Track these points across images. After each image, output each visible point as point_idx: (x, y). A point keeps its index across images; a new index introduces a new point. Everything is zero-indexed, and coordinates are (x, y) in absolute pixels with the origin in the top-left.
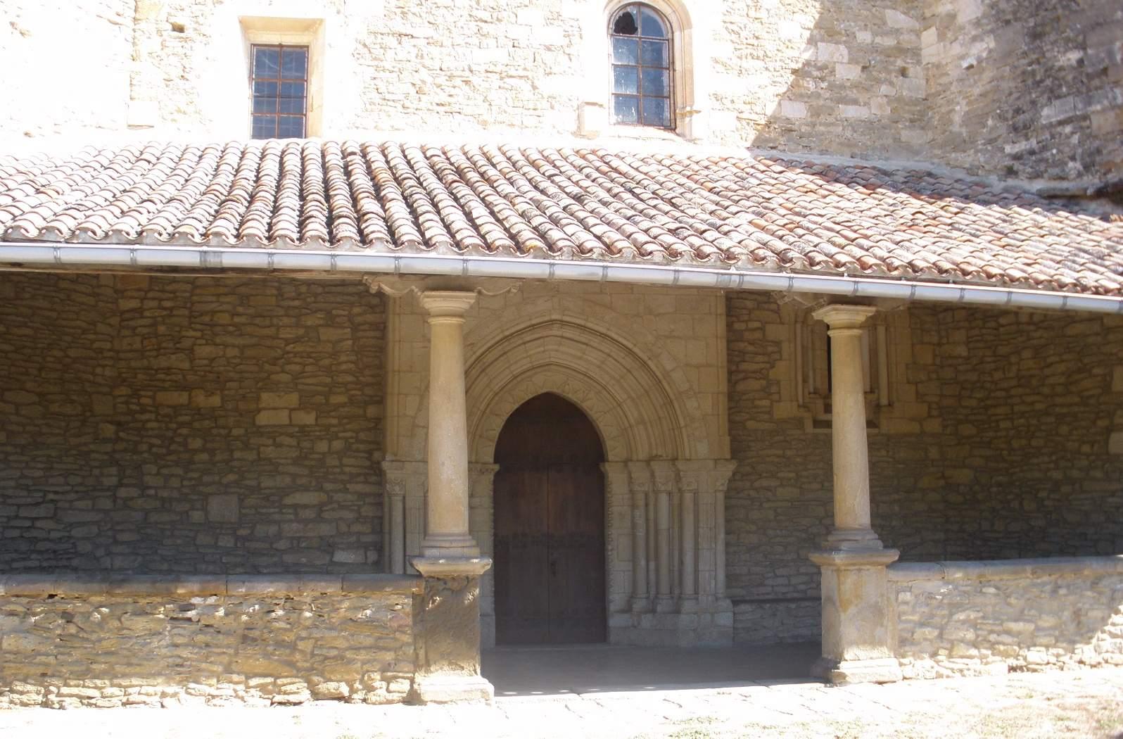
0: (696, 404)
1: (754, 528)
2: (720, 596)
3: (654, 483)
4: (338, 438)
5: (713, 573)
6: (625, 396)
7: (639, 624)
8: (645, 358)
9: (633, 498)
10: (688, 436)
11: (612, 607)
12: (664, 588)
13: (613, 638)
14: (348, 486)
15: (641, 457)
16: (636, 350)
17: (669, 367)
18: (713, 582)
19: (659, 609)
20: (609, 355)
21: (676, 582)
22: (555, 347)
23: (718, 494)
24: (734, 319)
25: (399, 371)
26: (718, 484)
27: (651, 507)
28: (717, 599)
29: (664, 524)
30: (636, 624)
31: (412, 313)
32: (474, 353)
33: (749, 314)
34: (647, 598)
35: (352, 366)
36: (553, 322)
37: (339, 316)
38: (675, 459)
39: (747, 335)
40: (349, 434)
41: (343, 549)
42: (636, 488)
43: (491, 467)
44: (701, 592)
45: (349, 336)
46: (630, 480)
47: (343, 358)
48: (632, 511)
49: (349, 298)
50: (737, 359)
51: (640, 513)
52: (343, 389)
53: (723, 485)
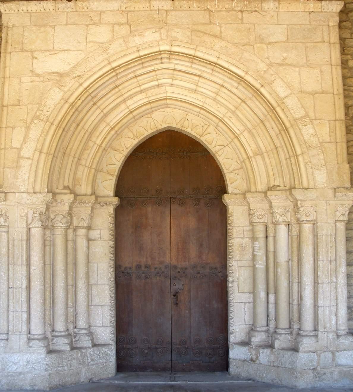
0: (312, 131)
2: (341, 332)
3: (272, 213)
5: (334, 309)
6: (242, 128)
7: (257, 358)
8: (258, 86)
9: (253, 231)
10: (306, 164)
11: (232, 339)
13: (232, 369)
15: (259, 188)
17: (282, 94)
18: (334, 318)
19: (277, 344)
20: (222, 86)
21: (295, 318)
22: (169, 81)
25: (7, 106)
26: (338, 214)
27: (271, 239)
28: (338, 336)
29: (283, 256)
30: (254, 357)
31: (22, 50)
32: (81, 85)
34: (267, 331)
38: (291, 189)
42: (256, 220)
43: (110, 200)
44: (321, 329)
51: (260, 244)
53: (343, 215)
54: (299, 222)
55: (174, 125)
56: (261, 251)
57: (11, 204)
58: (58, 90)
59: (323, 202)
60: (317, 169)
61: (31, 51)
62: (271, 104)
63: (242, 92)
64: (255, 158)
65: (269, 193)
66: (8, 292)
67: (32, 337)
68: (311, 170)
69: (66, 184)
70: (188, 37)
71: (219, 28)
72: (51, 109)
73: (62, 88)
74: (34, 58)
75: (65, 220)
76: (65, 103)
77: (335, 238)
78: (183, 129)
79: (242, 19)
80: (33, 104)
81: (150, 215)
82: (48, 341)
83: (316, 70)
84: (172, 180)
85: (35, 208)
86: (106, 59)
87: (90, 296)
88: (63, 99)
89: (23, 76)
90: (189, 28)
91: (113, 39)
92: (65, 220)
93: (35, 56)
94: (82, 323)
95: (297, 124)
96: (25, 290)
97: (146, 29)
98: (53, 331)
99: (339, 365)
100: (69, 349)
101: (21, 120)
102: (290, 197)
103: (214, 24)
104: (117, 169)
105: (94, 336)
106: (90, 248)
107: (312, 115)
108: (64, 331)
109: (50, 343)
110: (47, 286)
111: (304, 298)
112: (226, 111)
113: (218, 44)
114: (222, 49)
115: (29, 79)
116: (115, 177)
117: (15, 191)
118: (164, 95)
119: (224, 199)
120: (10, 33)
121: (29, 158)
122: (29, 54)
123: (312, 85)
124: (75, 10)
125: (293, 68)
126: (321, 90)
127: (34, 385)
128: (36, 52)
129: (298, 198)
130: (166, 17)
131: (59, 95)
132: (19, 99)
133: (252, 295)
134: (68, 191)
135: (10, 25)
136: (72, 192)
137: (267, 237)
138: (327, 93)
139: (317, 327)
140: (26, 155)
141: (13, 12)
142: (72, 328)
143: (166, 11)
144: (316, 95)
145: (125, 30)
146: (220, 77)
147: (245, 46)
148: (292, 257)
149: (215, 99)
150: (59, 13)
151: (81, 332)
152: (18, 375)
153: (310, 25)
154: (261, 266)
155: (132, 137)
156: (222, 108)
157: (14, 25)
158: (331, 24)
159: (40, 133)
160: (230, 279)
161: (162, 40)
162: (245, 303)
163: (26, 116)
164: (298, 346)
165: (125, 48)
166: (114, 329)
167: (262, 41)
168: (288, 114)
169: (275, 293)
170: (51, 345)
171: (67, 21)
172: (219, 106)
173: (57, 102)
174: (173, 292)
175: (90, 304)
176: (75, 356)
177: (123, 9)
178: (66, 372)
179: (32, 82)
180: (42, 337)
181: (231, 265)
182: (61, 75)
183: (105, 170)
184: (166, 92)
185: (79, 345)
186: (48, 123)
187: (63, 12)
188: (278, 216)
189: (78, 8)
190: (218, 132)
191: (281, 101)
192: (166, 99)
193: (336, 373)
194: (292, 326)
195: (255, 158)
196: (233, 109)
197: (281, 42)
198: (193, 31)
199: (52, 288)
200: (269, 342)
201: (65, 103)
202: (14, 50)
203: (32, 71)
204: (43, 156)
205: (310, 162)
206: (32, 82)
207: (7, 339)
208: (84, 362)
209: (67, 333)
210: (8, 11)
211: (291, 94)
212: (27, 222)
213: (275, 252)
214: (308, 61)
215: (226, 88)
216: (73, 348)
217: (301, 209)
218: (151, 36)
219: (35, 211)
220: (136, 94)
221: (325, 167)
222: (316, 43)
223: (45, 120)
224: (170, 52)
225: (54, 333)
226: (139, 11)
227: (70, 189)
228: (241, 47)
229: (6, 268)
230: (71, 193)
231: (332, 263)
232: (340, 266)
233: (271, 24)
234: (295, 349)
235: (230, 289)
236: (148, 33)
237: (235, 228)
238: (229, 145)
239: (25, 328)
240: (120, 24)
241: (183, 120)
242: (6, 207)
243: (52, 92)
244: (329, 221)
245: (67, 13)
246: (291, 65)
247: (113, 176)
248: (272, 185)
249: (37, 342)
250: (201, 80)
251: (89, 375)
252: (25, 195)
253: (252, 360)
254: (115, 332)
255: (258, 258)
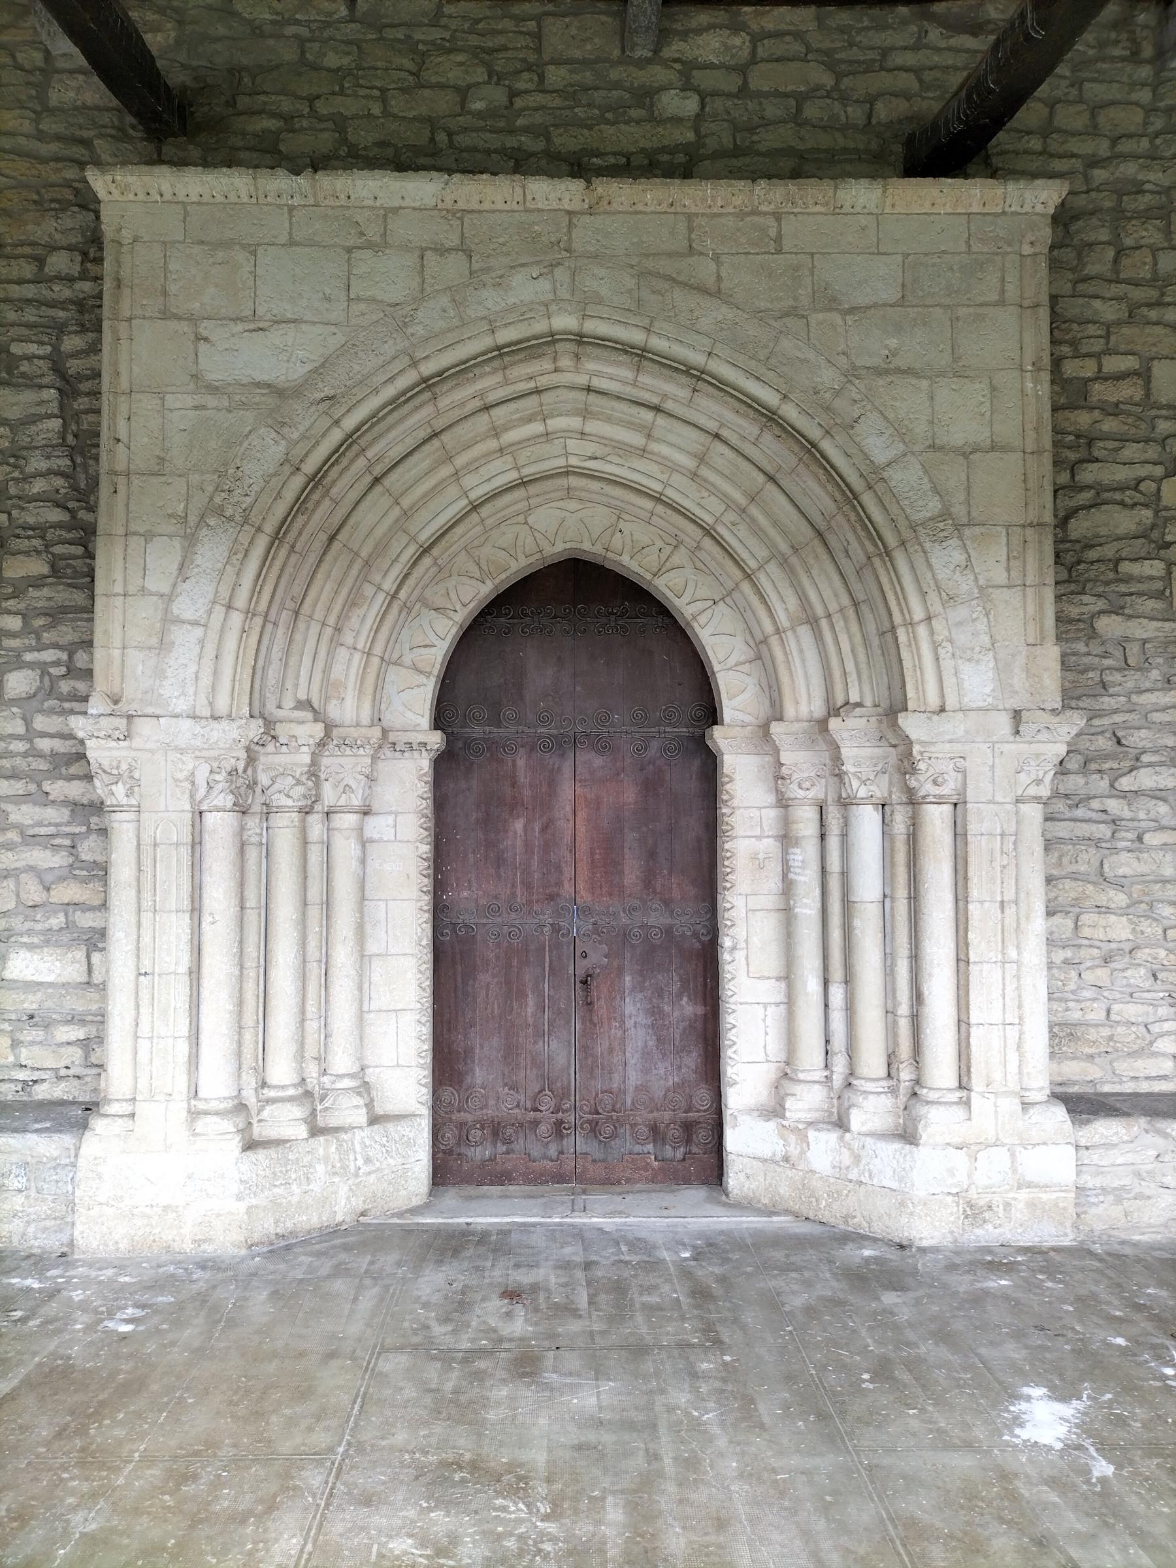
1: (1120, 899)
3: (840, 776)
4: (21, 665)
8: (814, 433)
12: (872, 1061)
13: (734, 1180)
14: (47, 786)
16: (790, 412)
18: (1013, 1057)
19: (857, 1120)
23: (1024, 808)
24: (1066, 349)
31: (166, 315)
33: (1107, 337)
35: (59, 482)
36: (553, 338)
37: (29, 358)
39: (1099, 391)
40: (49, 655)
41: (31, 947)
43: (421, 738)
44: (977, 1084)
45: (54, 408)
46: (778, 776)
47: (37, 463)
48: (785, 852)
49: (51, 312)
50: (1072, 456)
52: (36, 542)
53: (1038, 782)
54: (913, 801)
55: (586, 546)
56: (808, 872)
57: (148, 746)
58: (274, 435)
59: (985, 746)
60: (969, 660)
61: (193, 319)
62: (847, 485)
63: (772, 450)
64: (795, 632)
65: (834, 723)
66: (137, 985)
67: (201, 1106)
68: (952, 662)
69: (302, 696)
70: (630, 291)
71: (713, 266)
72: (255, 488)
73: (286, 430)
74: (199, 338)
75: (300, 790)
76: (292, 473)
77: (1015, 843)
78: (610, 555)
79: (778, 239)
80: (203, 473)
81: (523, 778)
82: (249, 1115)
83: (977, 386)
84: (578, 688)
85: (215, 759)
86: (404, 352)
87: (366, 986)
88: (287, 460)
89: (169, 389)
90: (632, 267)
91: (421, 296)
92: (300, 790)
93: (205, 333)
94: (342, 1061)
95: (917, 538)
96: (187, 978)
97: (512, 267)
98: (264, 1084)
99: (1029, 1185)
100: (305, 1135)
101: (170, 516)
102: (889, 735)
103: (701, 254)
104: (440, 659)
105: (374, 1093)
106: (369, 861)
107: (959, 510)
108: (294, 1086)
109: (254, 1121)
110: (248, 964)
111: (927, 1001)
112: (723, 507)
113: (712, 314)
114: (722, 329)
115: (190, 401)
116: (433, 680)
117: (158, 712)
118: (561, 462)
119: (711, 737)
120: (126, 259)
121: (196, 623)
122: (184, 327)
123: (964, 428)
124: (312, 202)
125: (914, 381)
126: (988, 442)
127: (205, 1241)
128: (206, 323)
129: (913, 737)
130: (569, 232)
131: (277, 451)
132: (162, 455)
133: (783, 985)
134: (309, 715)
135: (126, 235)
136: (318, 716)
137: (823, 837)
138: (1005, 449)
139: (965, 1079)
140: (188, 615)
141: (131, 197)
142: (315, 1075)
143: (569, 213)
144: (975, 457)
145: (453, 268)
146: (711, 410)
147: (787, 320)
148: (893, 889)
149: (694, 476)
150: (266, 208)
151: (339, 1085)
152: (159, 1211)
153: (969, 252)
154: (808, 912)
155: (478, 575)
156: (713, 498)
157: (136, 239)
158: (1027, 250)
159: (226, 554)
160: (726, 942)
161: (557, 300)
162: (765, 1005)
163: (182, 506)
164: (916, 1128)
165: (456, 322)
166: (427, 1072)
167: (831, 303)
168: (894, 509)
169: (846, 982)
170: (255, 1125)
171: (290, 234)
172: (706, 494)
173: (271, 471)
174: (581, 973)
175: (365, 1008)
176: (321, 1151)
177: (449, 204)
178: (295, 1200)
179: (196, 408)
180: (230, 1104)
181: (728, 905)
182: (278, 392)
183: (407, 660)
184: (567, 455)
185: (333, 1121)
186: (246, 527)
187: (279, 206)
188: (855, 784)
189: (321, 196)
190: (699, 564)
191: (875, 476)
192: (567, 473)
193: (1021, 1206)
194: (894, 1072)
195: (795, 632)
196: (742, 501)
197: (885, 305)
198: (643, 274)
199: (262, 971)
200: (831, 1113)
201: (292, 473)
202: (139, 312)
203: (195, 377)
204: (236, 619)
205: (951, 641)
206: (196, 408)
207: (133, 1115)
208: (345, 1168)
209: (300, 1091)
210: (116, 194)
211: (905, 455)
212: (192, 796)
213: (845, 875)
214: (956, 360)
215: (725, 442)
216: (316, 1131)
217: (922, 766)
218: (526, 288)
219: (215, 765)
220: (487, 457)
221: (991, 654)
222: (981, 305)
223: (238, 518)
224: (580, 339)
225: (266, 1091)
226: (494, 212)
227: (314, 710)
228: (772, 322)
229: (133, 920)
230: (316, 720)
231: (1007, 911)
232: (1028, 918)
233: (859, 254)
234: (907, 1135)
235: (728, 967)
236: (517, 279)
237: (738, 812)
238: (728, 600)
239: (181, 1084)
240: (442, 251)
241: (609, 531)
242: (133, 754)
243: (254, 440)
244: (999, 798)
245: (291, 209)
246: (908, 372)
247: (428, 674)
248: (839, 704)
249: (216, 1119)
250: (661, 421)
251: (359, 1204)
252: (187, 724)
253: (786, 1159)
254: (429, 1080)
255: (800, 890)
